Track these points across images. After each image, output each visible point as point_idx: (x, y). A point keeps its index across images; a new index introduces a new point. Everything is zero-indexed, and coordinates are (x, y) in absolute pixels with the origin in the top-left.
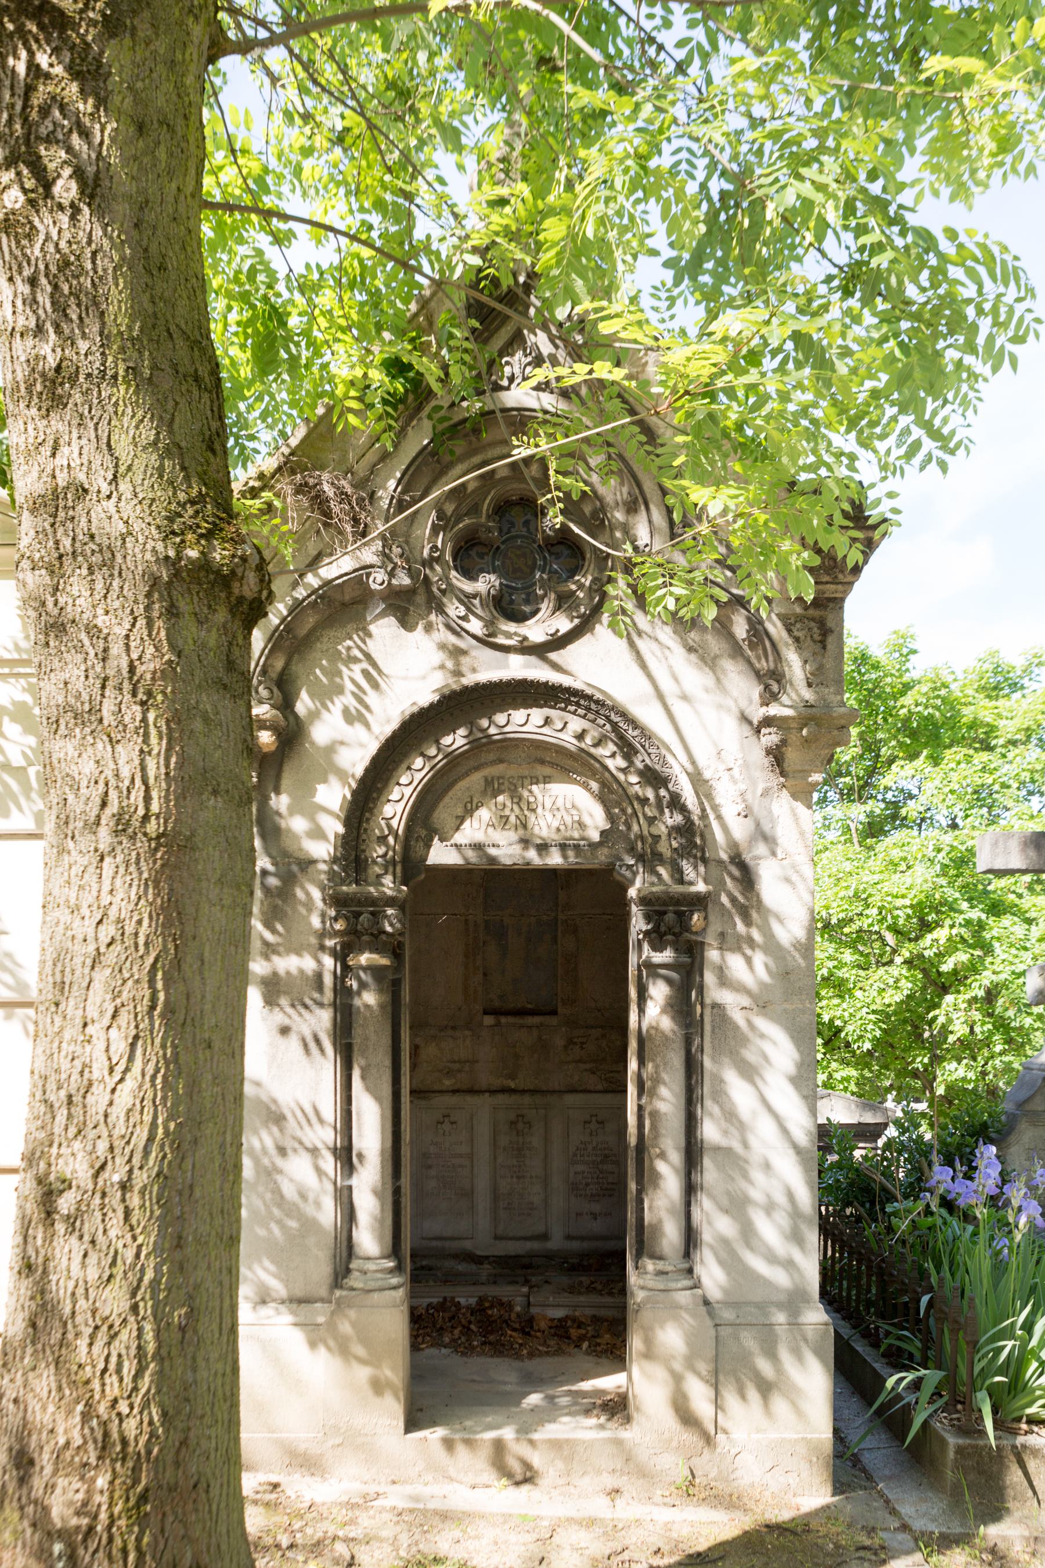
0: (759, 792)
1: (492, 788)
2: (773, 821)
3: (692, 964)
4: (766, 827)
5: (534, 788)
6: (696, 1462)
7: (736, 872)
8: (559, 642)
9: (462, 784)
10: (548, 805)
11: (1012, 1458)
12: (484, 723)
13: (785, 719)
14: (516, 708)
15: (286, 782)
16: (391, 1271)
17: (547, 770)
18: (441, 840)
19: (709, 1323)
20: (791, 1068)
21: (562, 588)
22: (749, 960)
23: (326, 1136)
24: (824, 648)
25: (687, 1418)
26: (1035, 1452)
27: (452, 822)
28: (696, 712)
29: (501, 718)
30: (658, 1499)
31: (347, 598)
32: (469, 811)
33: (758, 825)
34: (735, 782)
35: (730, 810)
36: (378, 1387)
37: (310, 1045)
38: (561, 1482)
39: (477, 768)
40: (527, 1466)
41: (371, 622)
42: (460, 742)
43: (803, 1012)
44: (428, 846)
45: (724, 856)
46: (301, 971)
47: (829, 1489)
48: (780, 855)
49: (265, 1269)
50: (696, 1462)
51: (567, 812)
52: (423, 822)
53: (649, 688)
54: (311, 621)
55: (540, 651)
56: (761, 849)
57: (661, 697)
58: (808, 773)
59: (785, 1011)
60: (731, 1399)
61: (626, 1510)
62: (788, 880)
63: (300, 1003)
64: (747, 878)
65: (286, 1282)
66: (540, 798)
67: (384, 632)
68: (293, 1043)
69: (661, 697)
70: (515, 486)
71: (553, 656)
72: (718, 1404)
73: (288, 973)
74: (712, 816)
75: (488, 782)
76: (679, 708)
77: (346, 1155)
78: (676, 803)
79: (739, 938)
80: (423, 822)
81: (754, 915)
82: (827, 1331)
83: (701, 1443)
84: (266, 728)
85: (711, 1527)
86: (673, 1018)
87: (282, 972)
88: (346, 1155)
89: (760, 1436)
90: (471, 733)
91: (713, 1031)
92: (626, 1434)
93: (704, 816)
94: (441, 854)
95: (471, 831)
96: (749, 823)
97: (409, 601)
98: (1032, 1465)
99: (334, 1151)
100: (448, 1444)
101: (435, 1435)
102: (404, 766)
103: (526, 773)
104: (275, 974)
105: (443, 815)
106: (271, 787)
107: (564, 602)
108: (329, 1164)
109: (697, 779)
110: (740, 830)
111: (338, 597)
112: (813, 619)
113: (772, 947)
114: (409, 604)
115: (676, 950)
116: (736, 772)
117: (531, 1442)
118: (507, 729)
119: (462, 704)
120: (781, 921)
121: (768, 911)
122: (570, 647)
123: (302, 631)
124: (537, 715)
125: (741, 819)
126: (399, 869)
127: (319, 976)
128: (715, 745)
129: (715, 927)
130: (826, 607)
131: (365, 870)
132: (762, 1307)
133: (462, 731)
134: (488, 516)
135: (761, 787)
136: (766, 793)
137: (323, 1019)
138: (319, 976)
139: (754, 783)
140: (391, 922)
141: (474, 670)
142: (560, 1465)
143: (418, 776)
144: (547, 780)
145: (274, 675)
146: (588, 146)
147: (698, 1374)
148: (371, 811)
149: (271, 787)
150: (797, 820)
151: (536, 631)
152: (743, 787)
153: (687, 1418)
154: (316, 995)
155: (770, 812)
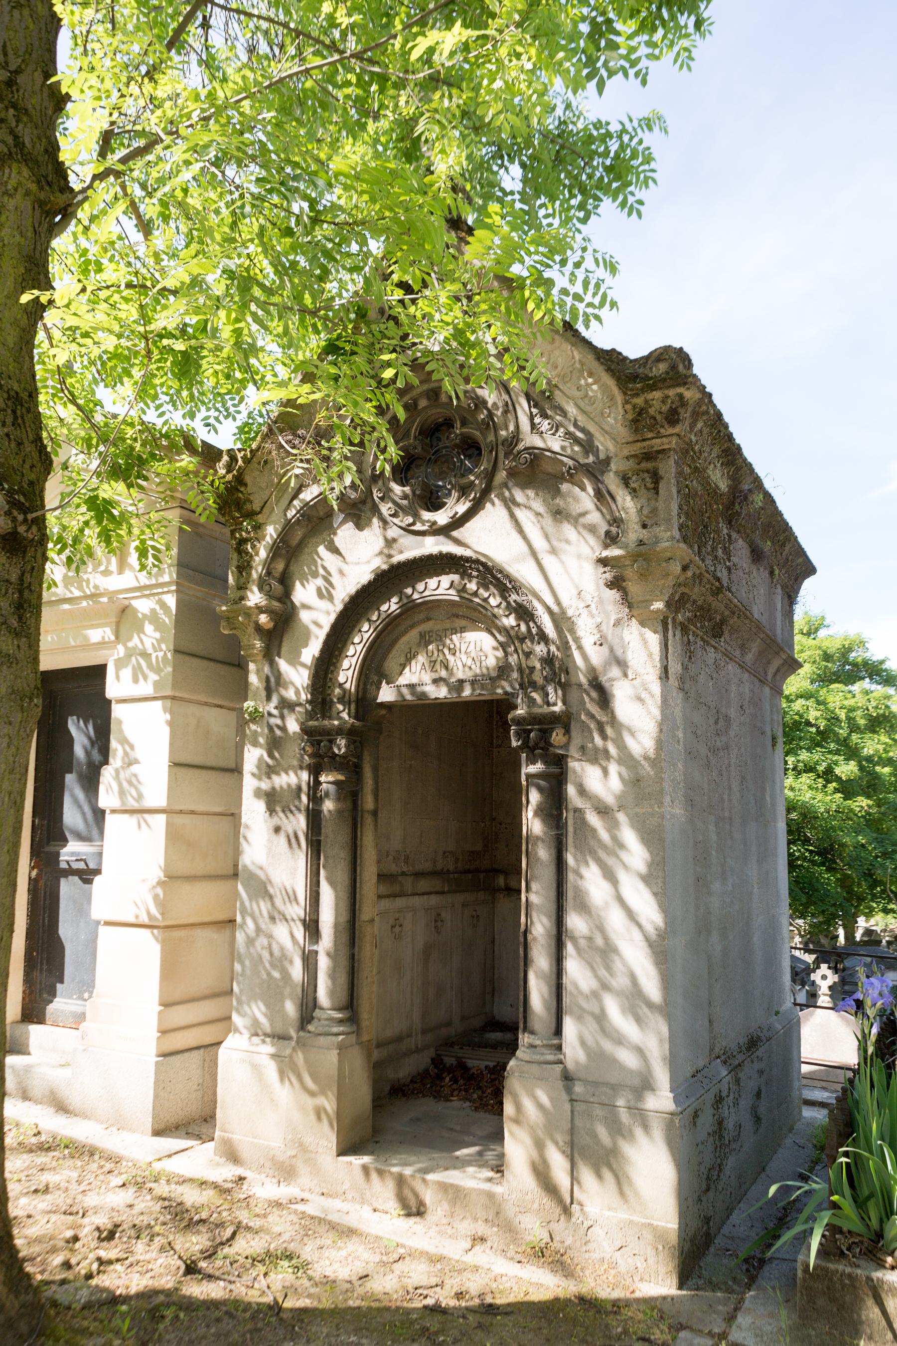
0: (612, 623)
1: (424, 640)
2: (624, 648)
3: (562, 773)
4: (619, 653)
5: (454, 637)
6: (554, 1226)
7: (594, 694)
8: (459, 522)
9: (404, 639)
10: (463, 650)
11: (867, 1290)
12: (409, 591)
13: (617, 558)
14: (431, 577)
15: (284, 649)
16: (341, 1021)
17: (463, 623)
18: (388, 683)
19: (565, 1097)
20: (642, 868)
21: (464, 481)
22: (605, 772)
23: (297, 911)
24: (657, 493)
25: (549, 1186)
26: (892, 1289)
27: (397, 669)
28: (562, 562)
29: (420, 586)
30: (511, 1253)
31: (321, 514)
32: (409, 658)
33: (612, 650)
34: (593, 616)
35: (588, 640)
36: (319, 1112)
37: (292, 840)
38: (445, 1221)
39: (412, 626)
40: (421, 1204)
41: (338, 527)
42: (394, 607)
43: (653, 815)
44: (379, 688)
45: (583, 680)
46: (289, 786)
47: (674, 1281)
48: (630, 677)
49: (259, 1009)
50: (554, 1226)
51: (475, 652)
52: (374, 669)
53: (524, 548)
54: (299, 534)
55: (445, 531)
56: (615, 671)
57: (534, 554)
58: (650, 602)
59: (636, 814)
60: (587, 1175)
61: (481, 1256)
62: (640, 699)
63: (286, 810)
64: (604, 698)
65: (271, 1020)
66: (458, 645)
67: (345, 534)
68: (282, 839)
69: (534, 554)
70: (434, 411)
71: (455, 534)
72: (574, 1178)
73: (281, 787)
74: (574, 647)
75: (422, 636)
76: (549, 561)
77: (312, 927)
78: (543, 637)
79: (596, 749)
80: (374, 669)
81: (609, 731)
82: (672, 1121)
83: (558, 1210)
84: (262, 612)
85: (540, 1284)
86: (544, 821)
87: (277, 786)
88: (312, 927)
89: (611, 1213)
90: (400, 600)
91: (575, 833)
92: (498, 1189)
93: (566, 646)
94: (386, 694)
95: (409, 676)
96: (605, 649)
97: (360, 510)
98: (891, 1304)
99: (304, 922)
100: (365, 1169)
101: (358, 1161)
102: (357, 630)
103: (448, 626)
104: (273, 788)
105: (391, 664)
106: (275, 653)
107: (464, 491)
108: (299, 932)
109: (561, 619)
110: (597, 656)
111: (315, 513)
112: (648, 471)
113: (626, 759)
114: (359, 510)
115: (545, 763)
116: (593, 607)
117: (424, 1180)
118: (425, 594)
119: (394, 578)
120: (632, 734)
121: (621, 725)
122: (467, 525)
123: (294, 542)
124: (446, 580)
125: (597, 647)
126: (353, 706)
127: (299, 789)
128: (577, 587)
129: (576, 741)
130: (656, 459)
131: (330, 708)
132: (615, 1088)
133: (395, 600)
134: (415, 437)
135: (613, 617)
136: (618, 623)
137: (300, 822)
138: (299, 789)
139: (608, 617)
140: (341, 746)
141: (401, 552)
142: (446, 1206)
143: (366, 636)
144: (463, 630)
145: (277, 575)
146: (392, 187)
147: (556, 1143)
148: (335, 665)
149: (275, 653)
150: (645, 642)
151: (442, 518)
152: (599, 620)
153: (549, 1186)
154: (297, 803)
155: (622, 639)
